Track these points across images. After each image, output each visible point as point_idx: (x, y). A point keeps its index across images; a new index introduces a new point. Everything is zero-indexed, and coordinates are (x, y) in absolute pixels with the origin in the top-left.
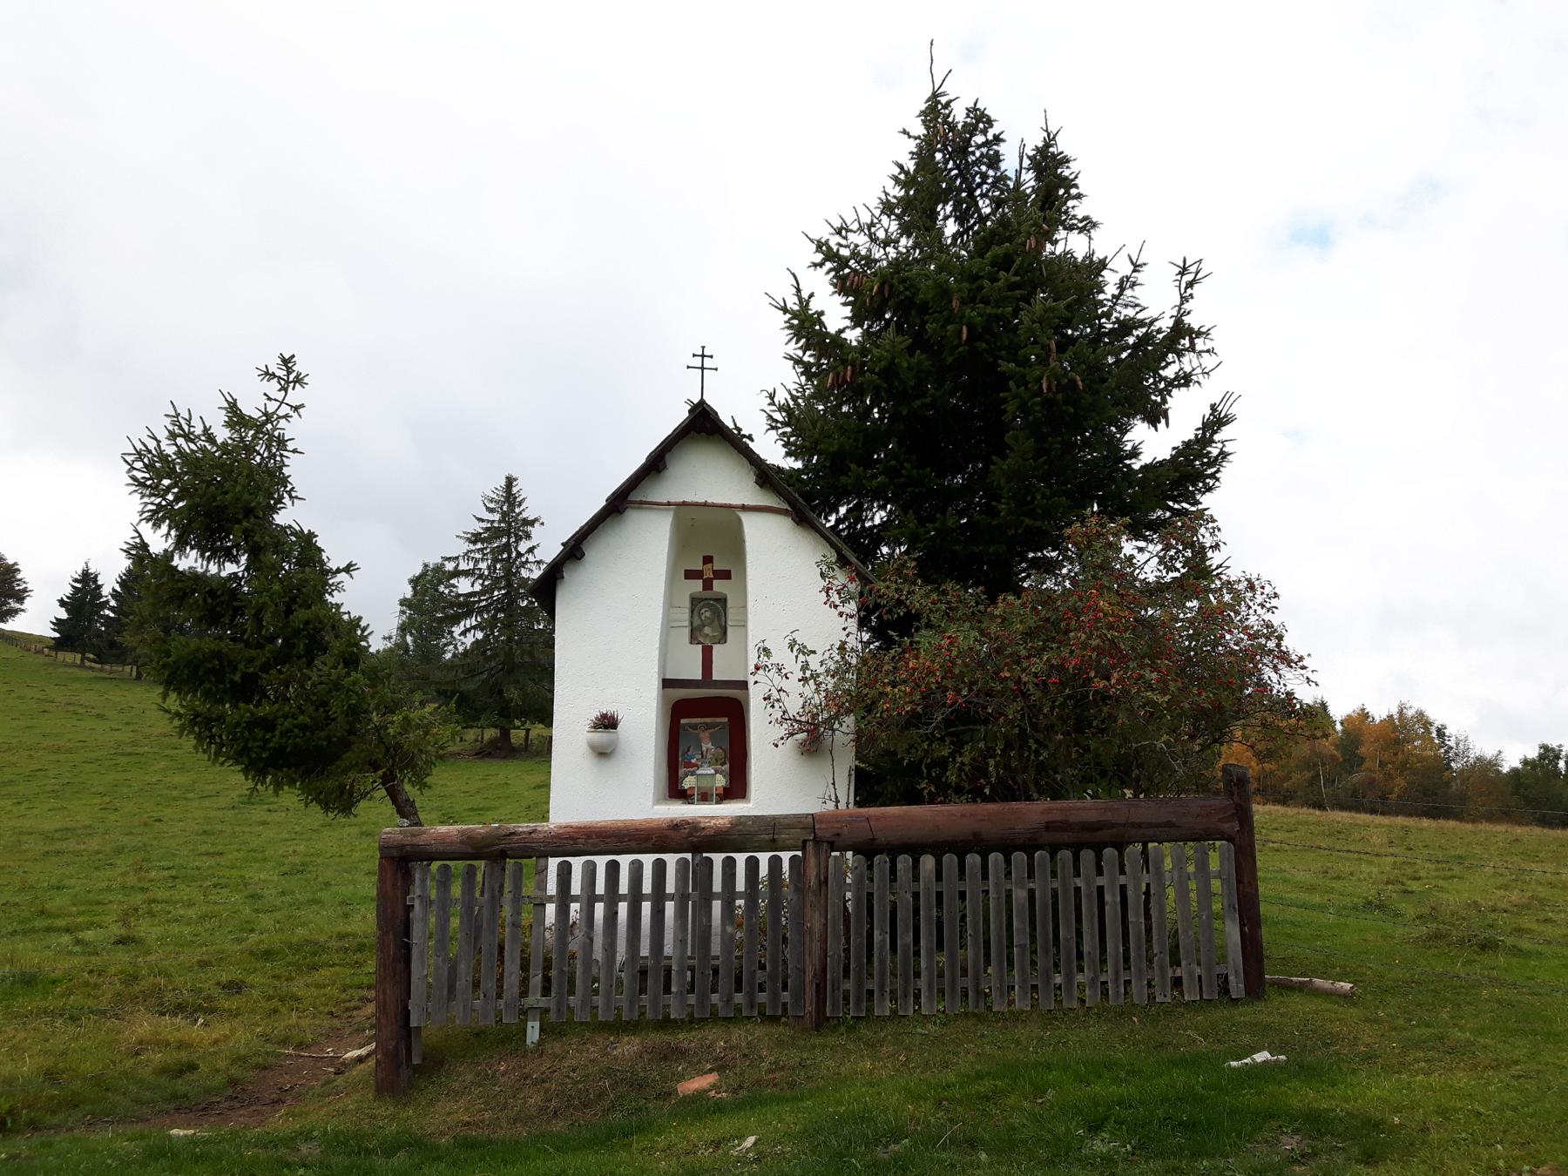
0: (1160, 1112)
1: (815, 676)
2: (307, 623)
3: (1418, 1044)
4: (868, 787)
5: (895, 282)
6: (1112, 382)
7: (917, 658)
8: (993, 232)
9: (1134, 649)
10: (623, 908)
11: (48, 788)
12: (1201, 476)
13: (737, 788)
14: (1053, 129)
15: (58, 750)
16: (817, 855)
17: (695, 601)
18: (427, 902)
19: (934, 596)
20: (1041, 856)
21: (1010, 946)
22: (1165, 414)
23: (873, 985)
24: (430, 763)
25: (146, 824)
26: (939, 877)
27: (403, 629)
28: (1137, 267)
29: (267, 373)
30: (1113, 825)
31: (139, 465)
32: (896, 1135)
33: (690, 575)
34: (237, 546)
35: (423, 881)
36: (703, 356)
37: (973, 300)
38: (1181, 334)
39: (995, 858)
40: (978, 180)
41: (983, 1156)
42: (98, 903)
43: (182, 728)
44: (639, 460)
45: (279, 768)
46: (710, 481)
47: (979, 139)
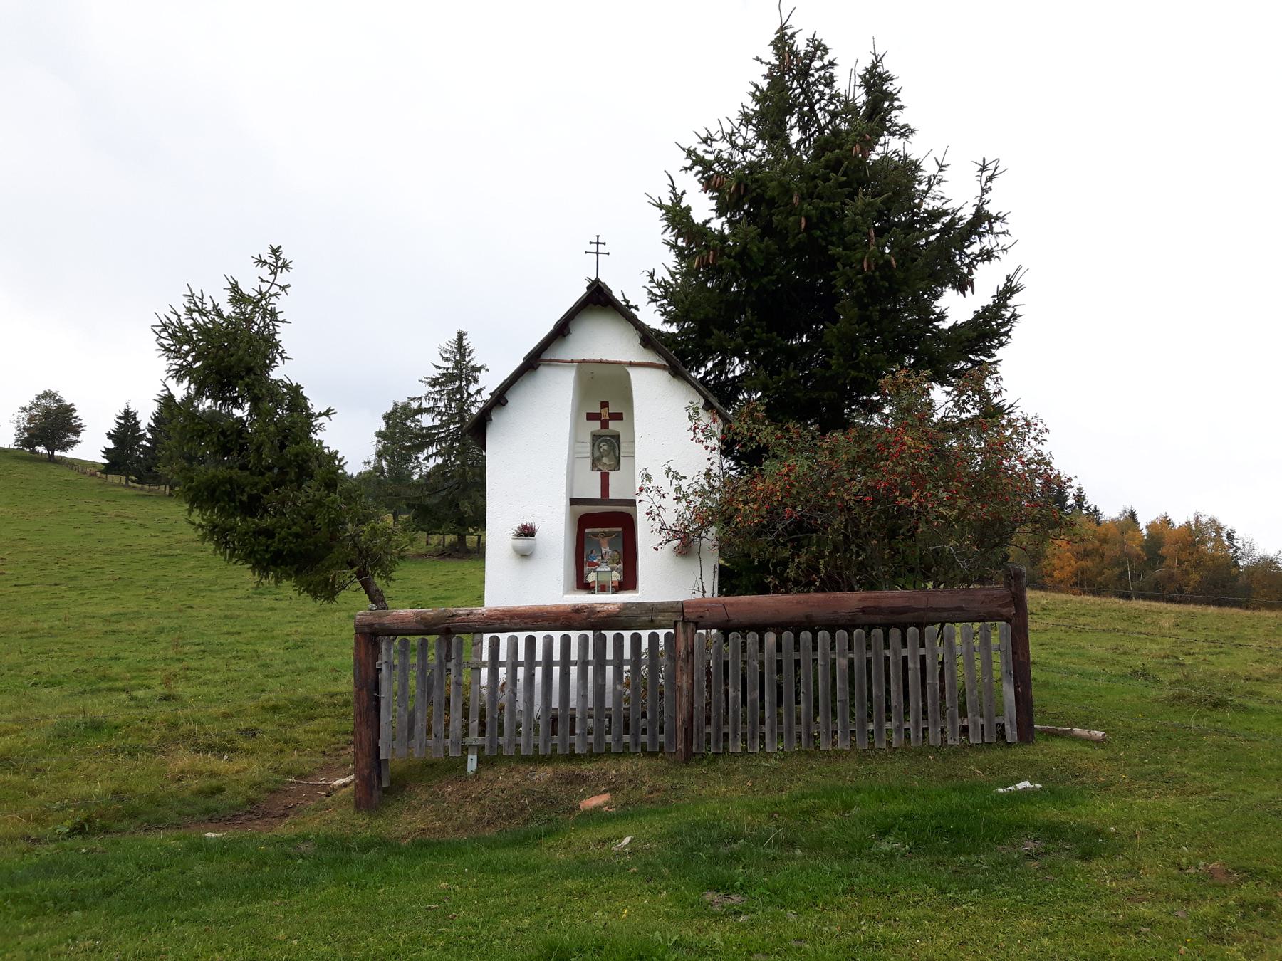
0: (933, 823)
1: (685, 496)
2: (297, 455)
3: (1144, 776)
4: (729, 580)
5: (749, 182)
6: (920, 261)
7: (764, 482)
8: (827, 140)
9: (930, 474)
10: (539, 671)
11: (105, 582)
12: (996, 334)
13: (629, 582)
14: (880, 52)
15: (111, 553)
16: (685, 632)
17: (595, 438)
18: (391, 667)
19: (779, 433)
20: (859, 634)
21: (834, 701)
22: (971, 283)
23: (728, 729)
24: (394, 563)
25: (180, 611)
26: (779, 649)
27: (380, 455)
28: (942, 167)
29: (260, 261)
30: (916, 610)
31: (164, 334)
32: (735, 837)
33: (591, 417)
34: (242, 396)
35: (388, 650)
36: (598, 243)
37: (811, 196)
38: (981, 216)
39: (841, 634)
40: (817, 96)
41: (798, 852)
42: (146, 670)
43: (203, 538)
44: (548, 327)
45: (277, 566)
46: (605, 343)
47: (817, 64)
